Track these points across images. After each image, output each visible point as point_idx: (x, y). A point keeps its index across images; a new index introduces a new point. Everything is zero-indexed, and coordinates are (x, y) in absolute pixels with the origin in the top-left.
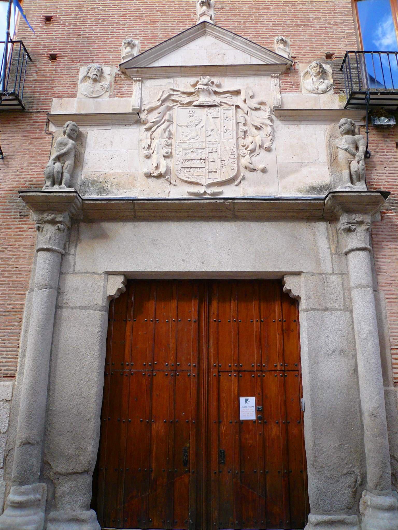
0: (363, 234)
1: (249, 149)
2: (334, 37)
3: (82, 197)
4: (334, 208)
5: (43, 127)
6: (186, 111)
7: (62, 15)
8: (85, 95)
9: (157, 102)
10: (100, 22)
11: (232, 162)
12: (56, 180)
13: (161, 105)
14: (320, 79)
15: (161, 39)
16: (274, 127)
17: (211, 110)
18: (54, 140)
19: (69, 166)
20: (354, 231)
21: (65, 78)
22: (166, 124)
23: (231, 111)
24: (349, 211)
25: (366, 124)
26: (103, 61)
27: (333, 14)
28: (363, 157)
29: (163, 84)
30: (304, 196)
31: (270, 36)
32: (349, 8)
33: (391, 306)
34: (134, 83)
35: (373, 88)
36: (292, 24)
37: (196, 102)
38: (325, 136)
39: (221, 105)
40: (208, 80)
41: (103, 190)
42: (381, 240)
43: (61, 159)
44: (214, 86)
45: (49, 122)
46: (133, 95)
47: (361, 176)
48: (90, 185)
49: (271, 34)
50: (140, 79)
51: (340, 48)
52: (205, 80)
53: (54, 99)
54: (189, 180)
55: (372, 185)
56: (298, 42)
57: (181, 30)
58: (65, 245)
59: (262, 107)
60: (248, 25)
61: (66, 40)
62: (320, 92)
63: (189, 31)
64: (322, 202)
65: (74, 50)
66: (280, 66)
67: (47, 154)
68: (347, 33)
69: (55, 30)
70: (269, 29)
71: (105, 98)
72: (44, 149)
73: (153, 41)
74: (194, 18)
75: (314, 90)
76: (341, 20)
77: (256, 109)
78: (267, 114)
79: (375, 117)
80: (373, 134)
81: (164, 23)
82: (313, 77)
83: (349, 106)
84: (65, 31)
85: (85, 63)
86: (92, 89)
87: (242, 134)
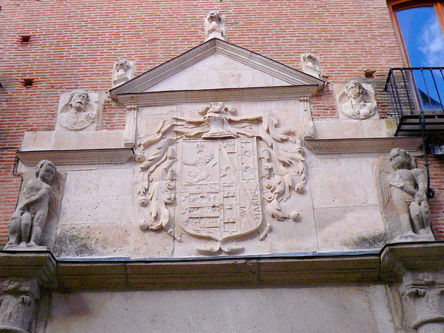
0: (436, 299)
1: (276, 191)
2: (373, 53)
3: (56, 258)
4: (394, 265)
5: (10, 168)
6: (193, 145)
7: (42, 35)
8: (66, 128)
9: (157, 135)
10: (88, 41)
11: (255, 210)
12: (23, 235)
13: (162, 138)
15: (161, 60)
16: (307, 161)
17: (225, 143)
18: (23, 184)
19: (41, 216)
20: (423, 295)
21: (41, 107)
22: (168, 161)
23: (251, 144)
24: (413, 269)
25: (423, 154)
26: (90, 86)
27: (369, 26)
28: (425, 196)
29: (165, 112)
30: (352, 251)
31: (294, 53)
32: (388, 20)
34: (127, 112)
35: (428, 110)
36: (321, 39)
37: (206, 134)
38: (373, 172)
39: (238, 137)
40: (220, 107)
41: (84, 248)
43: (31, 208)
44: (228, 113)
45: (18, 161)
46: (126, 127)
47: (425, 222)
48: (68, 241)
49: (296, 51)
50: (136, 106)
51: (382, 65)
52: (217, 106)
53: (26, 133)
54: (199, 234)
55: (441, 232)
56: (329, 59)
57: (187, 48)
58: (30, 324)
59: (291, 138)
60: (268, 41)
61: (46, 62)
62: (361, 117)
63: (196, 49)
64: (377, 258)
65: (55, 73)
66: (310, 88)
67: (13, 201)
68: (388, 47)
69: (34, 51)
70: (293, 45)
71: (91, 132)
72: (10, 195)
73: (151, 62)
74: (201, 35)
75: (353, 115)
76: (380, 33)
77: (283, 141)
78: (297, 147)
79: (435, 145)
80: (435, 167)
81: (165, 41)
82: (352, 99)
83: (400, 133)
84: (45, 52)
85: (66, 88)
86: (75, 120)
87: (267, 172)
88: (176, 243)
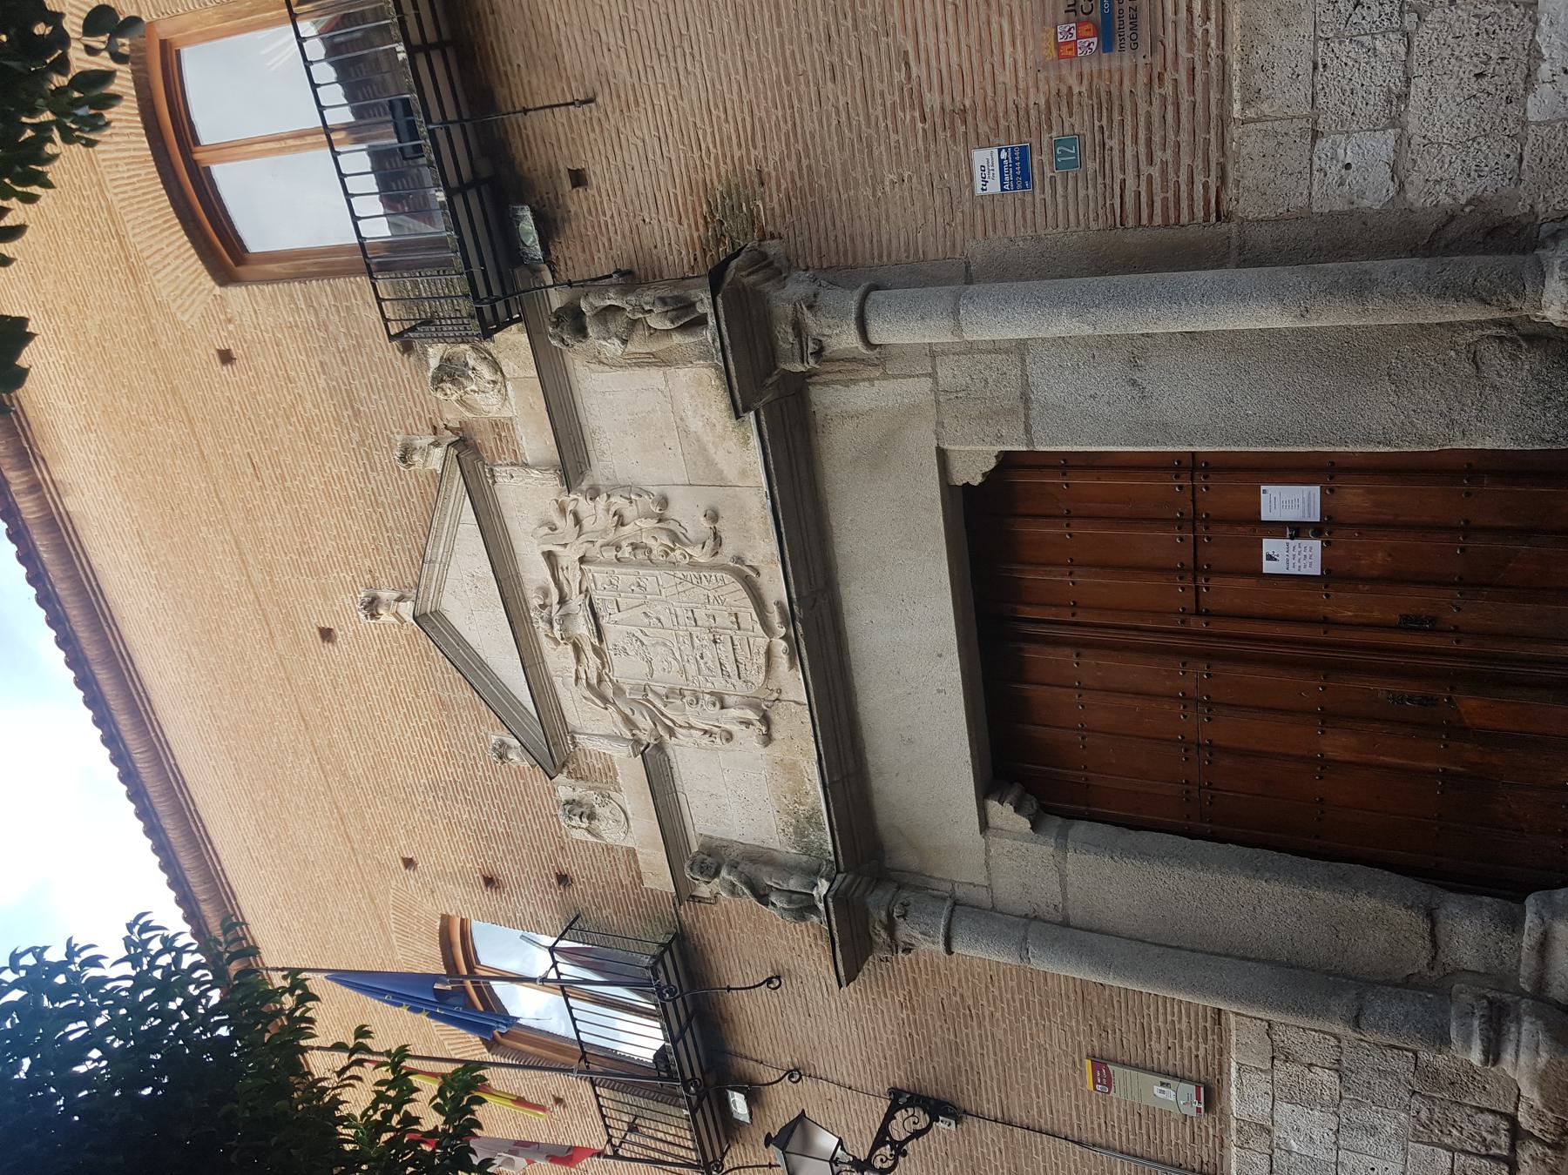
14: (468, 377)
17: (601, 613)
33: (1005, 222)
42: (832, 244)
45: (693, 897)
88: (783, 697)
